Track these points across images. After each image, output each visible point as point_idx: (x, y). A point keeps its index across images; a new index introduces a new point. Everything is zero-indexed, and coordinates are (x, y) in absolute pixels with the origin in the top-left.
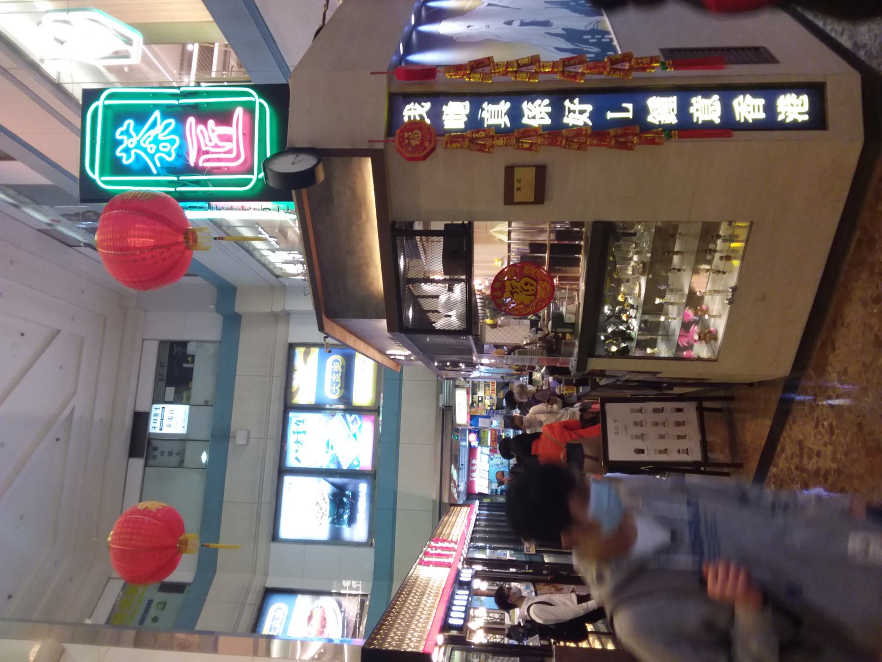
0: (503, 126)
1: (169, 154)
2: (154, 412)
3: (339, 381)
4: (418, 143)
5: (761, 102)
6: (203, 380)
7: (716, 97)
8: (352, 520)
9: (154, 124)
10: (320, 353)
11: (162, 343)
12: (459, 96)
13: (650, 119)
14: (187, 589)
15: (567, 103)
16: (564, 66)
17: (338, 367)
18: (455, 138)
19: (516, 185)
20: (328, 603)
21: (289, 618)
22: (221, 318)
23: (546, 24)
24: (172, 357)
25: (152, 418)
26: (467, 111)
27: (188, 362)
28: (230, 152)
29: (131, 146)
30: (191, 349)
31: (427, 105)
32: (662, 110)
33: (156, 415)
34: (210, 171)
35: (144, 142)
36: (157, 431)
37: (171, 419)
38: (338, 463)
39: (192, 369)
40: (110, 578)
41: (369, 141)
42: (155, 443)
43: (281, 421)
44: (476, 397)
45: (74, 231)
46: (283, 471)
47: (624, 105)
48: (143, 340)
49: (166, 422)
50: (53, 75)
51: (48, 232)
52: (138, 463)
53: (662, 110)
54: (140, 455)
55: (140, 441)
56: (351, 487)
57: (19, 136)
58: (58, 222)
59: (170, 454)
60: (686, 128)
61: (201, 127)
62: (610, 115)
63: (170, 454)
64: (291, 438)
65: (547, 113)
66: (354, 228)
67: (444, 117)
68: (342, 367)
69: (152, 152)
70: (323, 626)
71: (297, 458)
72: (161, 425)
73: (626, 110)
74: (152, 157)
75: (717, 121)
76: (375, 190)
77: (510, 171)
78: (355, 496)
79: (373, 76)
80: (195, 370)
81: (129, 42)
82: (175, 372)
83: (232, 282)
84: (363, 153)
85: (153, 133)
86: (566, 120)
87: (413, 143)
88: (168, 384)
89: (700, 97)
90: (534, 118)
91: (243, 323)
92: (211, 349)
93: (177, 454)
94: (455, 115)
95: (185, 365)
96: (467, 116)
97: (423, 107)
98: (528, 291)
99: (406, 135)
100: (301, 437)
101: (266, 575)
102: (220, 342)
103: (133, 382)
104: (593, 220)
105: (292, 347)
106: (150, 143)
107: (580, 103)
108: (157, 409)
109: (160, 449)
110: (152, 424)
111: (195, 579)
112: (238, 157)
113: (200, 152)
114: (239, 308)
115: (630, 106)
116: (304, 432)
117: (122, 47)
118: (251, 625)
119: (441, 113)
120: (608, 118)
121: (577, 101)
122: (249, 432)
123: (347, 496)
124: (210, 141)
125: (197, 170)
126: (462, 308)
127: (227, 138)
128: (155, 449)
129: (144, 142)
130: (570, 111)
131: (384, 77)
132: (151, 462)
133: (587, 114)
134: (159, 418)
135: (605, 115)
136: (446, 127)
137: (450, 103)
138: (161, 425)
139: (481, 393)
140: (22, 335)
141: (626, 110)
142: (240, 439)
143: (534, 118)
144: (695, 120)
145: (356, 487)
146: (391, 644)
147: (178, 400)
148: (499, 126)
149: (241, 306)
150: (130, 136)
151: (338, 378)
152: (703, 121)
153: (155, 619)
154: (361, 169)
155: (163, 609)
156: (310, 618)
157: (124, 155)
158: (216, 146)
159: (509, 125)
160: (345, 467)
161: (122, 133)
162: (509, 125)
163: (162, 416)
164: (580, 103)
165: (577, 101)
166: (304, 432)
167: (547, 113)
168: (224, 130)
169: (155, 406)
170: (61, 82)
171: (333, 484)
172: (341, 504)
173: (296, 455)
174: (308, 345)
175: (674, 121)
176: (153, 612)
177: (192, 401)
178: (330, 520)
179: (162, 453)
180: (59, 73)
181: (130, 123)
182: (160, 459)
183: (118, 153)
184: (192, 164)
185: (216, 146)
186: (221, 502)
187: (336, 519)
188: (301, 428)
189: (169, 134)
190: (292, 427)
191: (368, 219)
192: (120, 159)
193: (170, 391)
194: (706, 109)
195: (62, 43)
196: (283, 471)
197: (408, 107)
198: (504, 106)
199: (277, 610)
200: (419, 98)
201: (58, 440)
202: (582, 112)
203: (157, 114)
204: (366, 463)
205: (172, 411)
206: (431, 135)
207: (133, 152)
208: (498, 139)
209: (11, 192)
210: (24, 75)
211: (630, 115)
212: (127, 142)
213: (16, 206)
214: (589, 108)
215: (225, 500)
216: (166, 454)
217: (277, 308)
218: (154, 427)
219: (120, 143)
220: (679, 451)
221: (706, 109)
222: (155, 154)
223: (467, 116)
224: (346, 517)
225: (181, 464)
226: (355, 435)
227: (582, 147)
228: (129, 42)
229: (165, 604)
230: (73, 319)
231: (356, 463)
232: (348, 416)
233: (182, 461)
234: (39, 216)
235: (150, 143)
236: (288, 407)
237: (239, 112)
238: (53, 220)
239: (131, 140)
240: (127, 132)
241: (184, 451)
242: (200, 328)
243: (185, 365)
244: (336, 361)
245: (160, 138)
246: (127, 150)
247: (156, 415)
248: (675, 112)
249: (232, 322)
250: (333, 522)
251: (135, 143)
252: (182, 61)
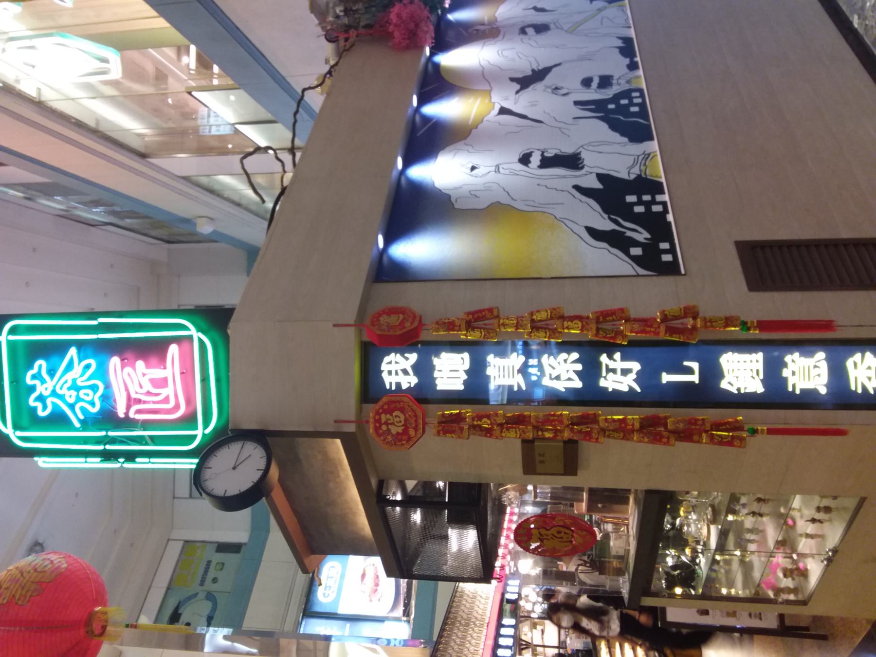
0: (516, 389)
1: (93, 404)
4: (400, 430)
7: (821, 355)
9: (70, 367)
12: (456, 346)
13: (724, 385)
14: (243, 549)
15: (604, 358)
16: (598, 321)
19: (538, 459)
21: (342, 576)
23: (572, 162)
26: (467, 366)
28: (166, 400)
29: (46, 393)
31: (413, 357)
32: (742, 372)
34: (146, 425)
35: (61, 388)
40: (169, 540)
41: (336, 422)
47: (686, 363)
50: (32, 92)
51: (66, 216)
53: (742, 372)
60: (776, 397)
62: (666, 378)
65: (576, 372)
66: (332, 485)
67: (436, 374)
69: (71, 401)
70: (377, 585)
73: (690, 371)
74: (72, 407)
75: (823, 391)
76: (350, 464)
79: (336, 329)
81: (105, 60)
85: (70, 376)
86: (603, 383)
87: (394, 430)
89: (797, 354)
90: (558, 378)
96: (466, 372)
97: (407, 359)
98: (561, 538)
99: (384, 418)
104: (645, 488)
106: (69, 389)
107: (623, 359)
111: (251, 537)
112: (177, 407)
113: (131, 401)
115: (695, 366)
118: (304, 594)
119: (432, 368)
120: (664, 381)
121: (617, 356)
124: (141, 387)
125: (127, 423)
127: (162, 383)
129: (61, 388)
130: (609, 370)
131: (353, 329)
133: (633, 376)
135: (659, 378)
136: (438, 388)
137: (444, 355)
141: (690, 371)
143: (558, 378)
144: (790, 389)
148: (511, 387)
150: (43, 381)
152: (801, 390)
153: (215, 580)
155: (222, 569)
156: (363, 576)
157: (39, 405)
158: (149, 393)
159: (524, 388)
161: (34, 377)
162: (524, 388)
164: (623, 359)
165: (617, 356)
167: (576, 372)
168: (157, 373)
170: (43, 99)
175: (760, 389)
176: (211, 574)
180: (39, 89)
183: (32, 402)
184: (121, 415)
185: (149, 393)
189: (88, 380)
192: (34, 409)
194: (807, 372)
195: (33, 67)
197: (387, 359)
202: (625, 372)
203: (73, 351)
207: (49, 401)
208: (508, 429)
209: (22, 189)
211: (695, 378)
212: (40, 389)
214: (636, 366)
219: (32, 389)
220: (750, 615)
221: (807, 372)
222: (76, 403)
223: (466, 372)
229: (223, 564)
230: (105, 295)
235: (69, 389)
239: (45, 386)
245: (79, 383)
246: (41, 398)
248: (761, 376)
251: (50, 389)
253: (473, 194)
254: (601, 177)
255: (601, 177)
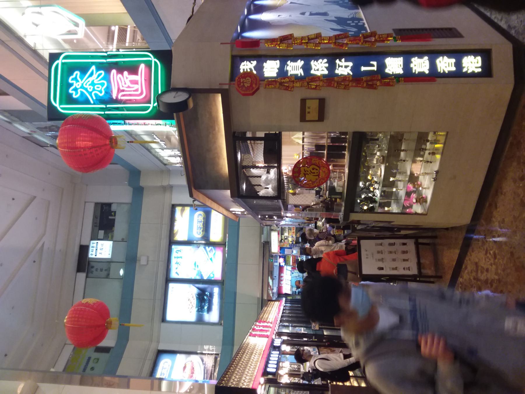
0: (299, 75)
1: (101, 92)
2: (91, 245)
3: (202, 227)
4: (249, 85)
5: (453, 61)
6: (121, 226)
7: (426, 58)
8: (209, 310)
9: (92, 74)
10: (190, 210)
11: (96, 204)
12: (273, 57)
13: (387, 71)
14: (111, 350)
15: (337, 61)
16: (336, 39)
17: (201, 218)
18: (271, 82)
19: (307, 110)
20: (195, 359)
21: (172, 368)
22: (131, 189)
23: (325, 14)
24: (102, 213)
25: (91, 249)
26: (278, 66)
27: (112, 215)
28: (137, 90)
29: (78, 87)
30: (114, 208)
31: (254, 63)
32: (394, 65)
33: (93, 247)
34: (125, 102)
35: (86, 85)
36: (94, 256)
37: (102, 250)
38: (201, 276)
39: (114, 220)
40: (65, 344)
41: (220, 84)
42: (92, 264)
43: (167, 250)
44: (283, 236)
45: (44, 138)
46: (168, 280)
47: (372, 62)
48: (85, 202)
49: (99, 251)
50: (32, 44)
51: (29, 138)
52: (82, 276)
53: (394, 65)
54: (83, 271)
55: (83, 262)
56: (209, 290)
57: (12, 81)
58: (35, 132)
59: (101, 270)
60: (409, 76)
61: (120, 76)
62: (363, 69)
63: (101, 270)
64: (173, 261)
65: (326, 67)
66: (211, 136)
67: (264, 70)
68: (204, 218)
69: (90, 90)
70: (193, 373)
71: (177, 273)
72: (96, 253)
73: (373, 66)
74: (90, 93)
75: (427, 72)
76: (223, 113)
77: (303, 102)
78: (211, 295)
79: (222, 45)
80: (116, 220)
81: (77, 25)
82: (104, 222)
83: (138, 168)
84: (216, 91)
85: (91, 79)
86: (337, 72)
87: (246, 85)
88: (100, 229)
89: (417, 58)
90: (318, 70)
91: (145, 192)
92: (126, 208)
93: (106, 270)
94: (271, 69)
95: (110, 217)
96: (278, 69)
97: (252, 63)
98: (314, 173)
99: (242, 80)
100: (179, 260)
101: (158, 342)
102: (131, 204)
103: (79, 227)
104: (353, 131)
105: (174, 207)
106: (89, 85)
107: (345, 61)
108: (93, 243)
109: (95, 267)
110: (90, 253)
111: (116, 344)
112: (142, 93)
113: (119, 91)
114: (142, 183)
115: (375, 63)
116: (181, 257)
117: (73, 28)
118: (149, 372)
119: (263, 67)
120: (362, 70)
121: (343, 60)
122: (148, 257)
123: (207, 295)
124: (125, 84)
125: (117, 101)
126: (275, 183)
127: (135, 82)
128: (93, 267)
129: (86, 85)
130: (339, 66)
131: (229, 46)
132: (90, 275)
133: (349, 68)
134: (95, 249)
135: (360, 69)
136: (265, 76)
137: (268, 61)
138: (96, 253)
139: (286, 234)
140: (13, 199)
141: (373, 66)
142: (143, 261)
143: (318, 70)
144: (414, 72)
145: (212, 290)
146: (233, 383)
147: (106, 238)
148: (297, 75)
149: (143, 182)
150: (77, 81)
151: (201, 225)
152: (418, 72)
153: (92, 369)
154: (215, 101)
155: (97, 362)
156: (185, 368)
157: (74, 92)
158: (129, 87)
159: (303, 74)
160: (205, 278)
161: (73, 79)
162: (303, 74)
163: (97, 247)
164: (345, 61)
165: (343, 60)
166: (181, 257)
167: (326, 67)
168: (133, 77)
169: (92, 242)
170: (36, 49)
171: (198, 288)
172: (203, 300)
173: (176, 271)
174: (183, 206)
175: (401, 72)
176: (91, 365)
177: (114, 239)
178: (196, 309)
179: (97, 270)
180: (35, 44)
181: (77, 73)
182: (95, 273)
183: (70, 91)
184: (114, 98)
185: (129, 87)
186: (132, 299)
187: (200, 309)
188: (179, 255)
189: (100, 80)
190: (174, 254)
191: (219, 131)
192: (72, 94)
193: (101, 233)
194: (420, 65)
195: (37, 25)
196: (168, 280)
197: (243, 64)
198: (300, 63)
199: (165, 363)
200: (249, 58)
201: (34, 262)
202: (346, 67)
203: (93, 68)
204: (218, 275)
205: (102, 245)
206: (257, 80)
207: (79, 91)
208: (296, 82)
209: (7, 114)
210: (14, 45)
211: (375, 68)
212: (75, 85)
213: (10, 123)
214: (351, 64)
215: (134, 297)
216: (99, 270)
217: (165, 183)
218: (92, 254)
219: (71, 85)
220: (404, 268)
221: (420, 65)
222: (92, 92)
223: (278, 69)
224: (206, 308)
225: (108, 276)
226: (211, 259)
227: (346, 87)
228: (77, 25)
229: (98, 359)
230: (43, 190)
231: (212, 276)
232: (207, 248)
233: (108, 275)
234: (23, 129)
235: (89, 85)
236: (172, 242)
237: (142, 66)
238: (32, 131)
239: (78, 83)
240: (75, 79)
241: (109, 268)
242: (119, 195)
243: (110, 217)
244: (200, 215)
245: (96, 82)
246: (76, 89)
247: (93, 247)
248: (402, 67)
249: (138, 192)
250: (198, 311)
251: (80, 85)
252: (108, 36)
253: (279, 21)
254: (335, 17)
255: (335, 17)
